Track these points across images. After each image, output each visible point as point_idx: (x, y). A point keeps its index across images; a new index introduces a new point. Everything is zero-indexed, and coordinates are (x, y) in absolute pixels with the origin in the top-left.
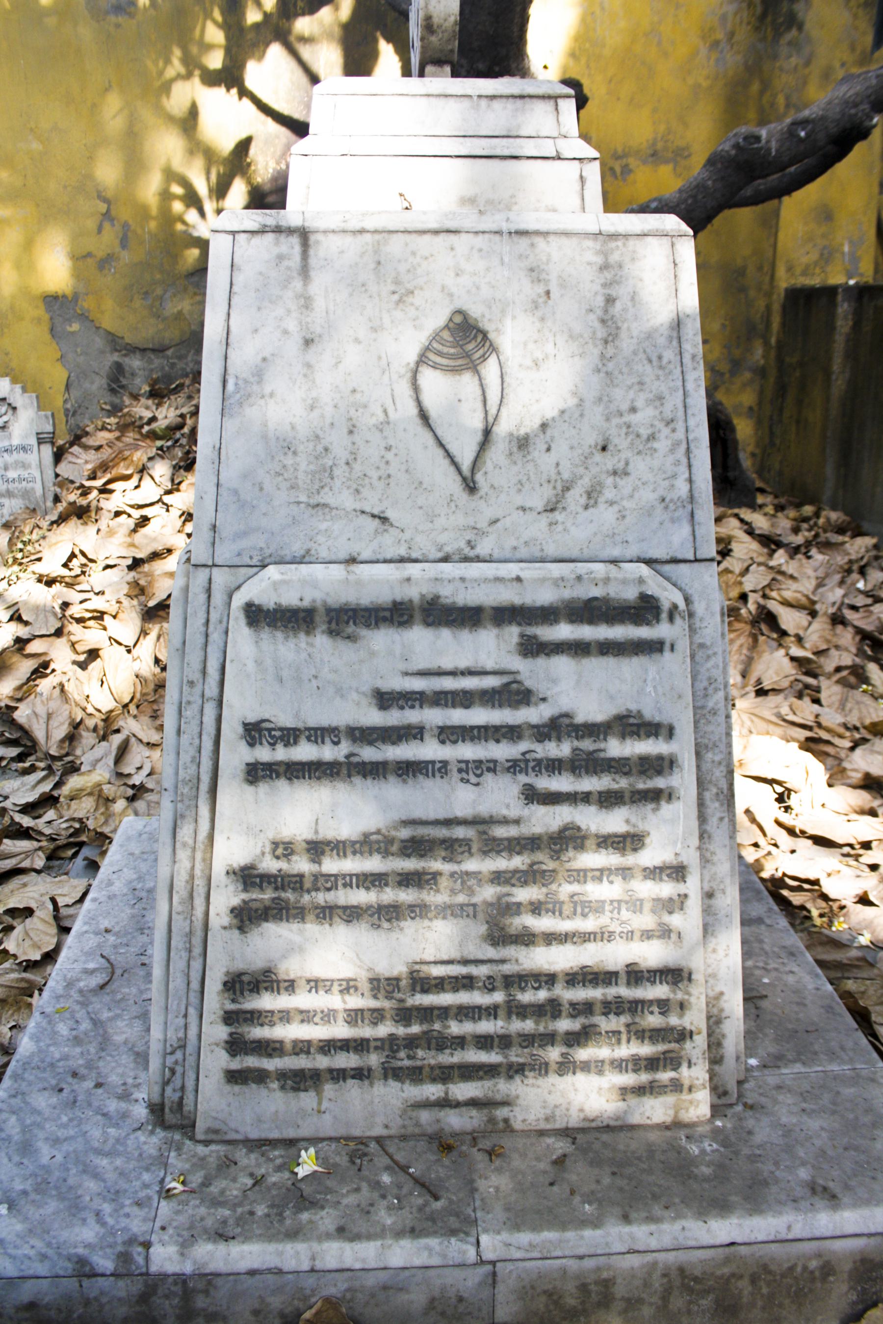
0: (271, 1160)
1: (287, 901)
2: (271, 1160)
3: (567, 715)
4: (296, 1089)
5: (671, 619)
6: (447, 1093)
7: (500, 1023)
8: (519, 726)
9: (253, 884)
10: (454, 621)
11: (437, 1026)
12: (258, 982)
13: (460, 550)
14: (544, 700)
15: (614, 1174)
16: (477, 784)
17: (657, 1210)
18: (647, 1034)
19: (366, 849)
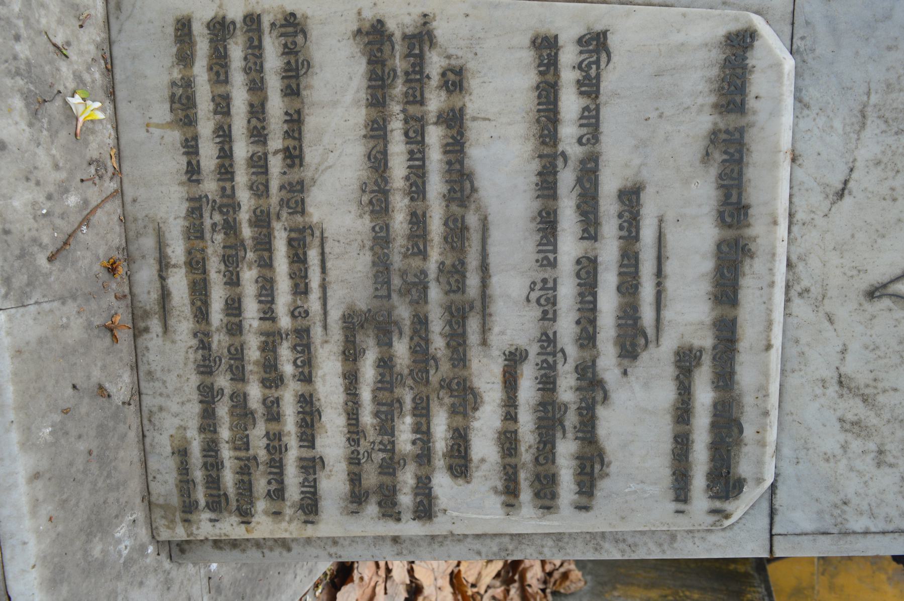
0: (88, 69)
1: (392, 86)
2: (88, 69)
3: (606, 398)
4: (172, 99)
5: (714, 512)
6: (175, 266)
7: (256, 324)
8: (595, 346)
9: (411, 47)
10: (722, 275)
11: (250, 255)
12: (297, 53)
13: (798, 280)
14: (625, 373)
15: (90, 453)
16: (528, 300)
17: (47, 509)
18: (246, 478)
19: (455, 177)
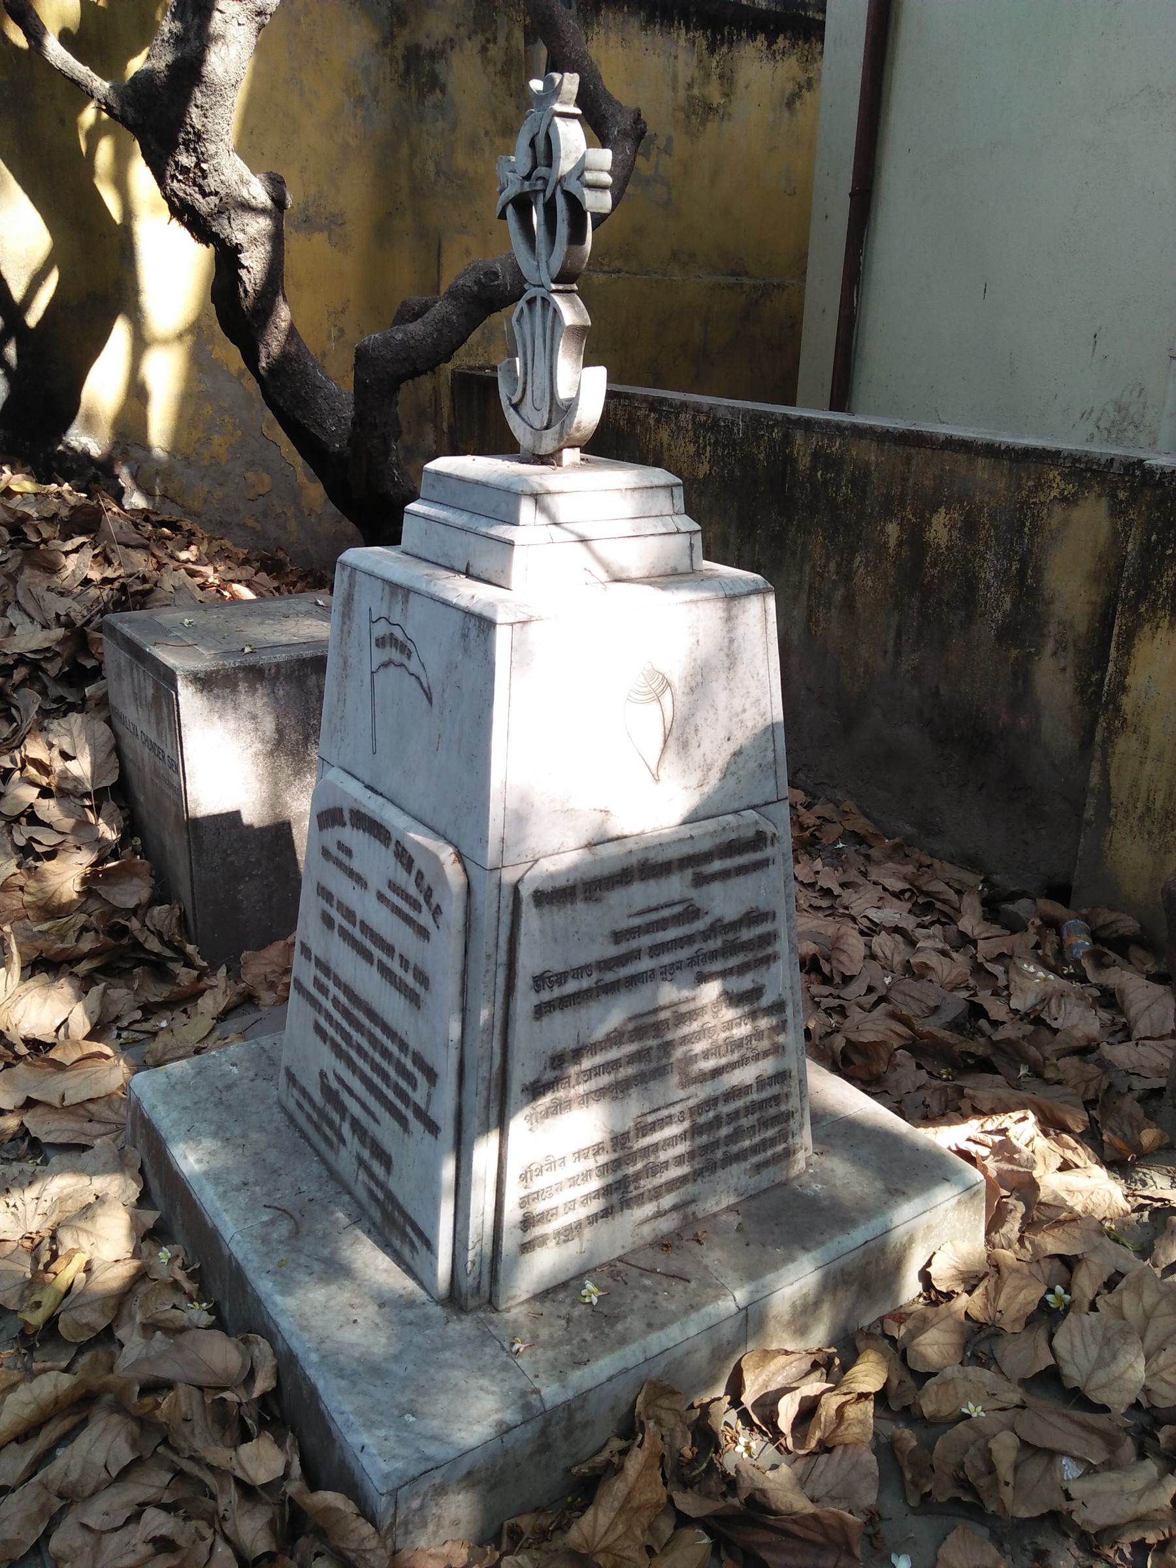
3: (719, 920)
11: (652, 1159)
